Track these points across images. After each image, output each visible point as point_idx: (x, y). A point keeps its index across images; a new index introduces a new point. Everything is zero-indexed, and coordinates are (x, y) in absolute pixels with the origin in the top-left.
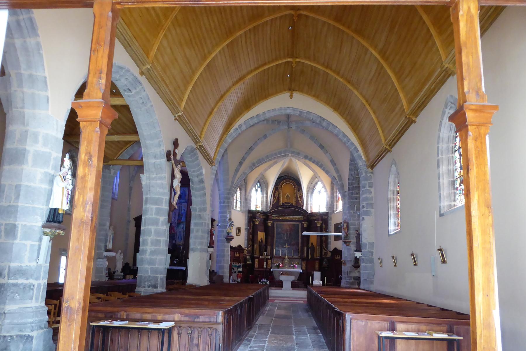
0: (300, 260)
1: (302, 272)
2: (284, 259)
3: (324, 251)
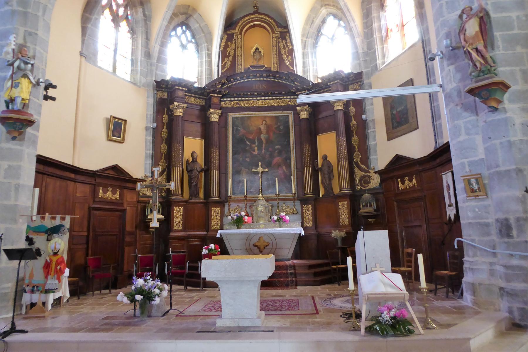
0: (298, 203)
1: (303, 233)
2: (255, 202)
3: (358, 173)
